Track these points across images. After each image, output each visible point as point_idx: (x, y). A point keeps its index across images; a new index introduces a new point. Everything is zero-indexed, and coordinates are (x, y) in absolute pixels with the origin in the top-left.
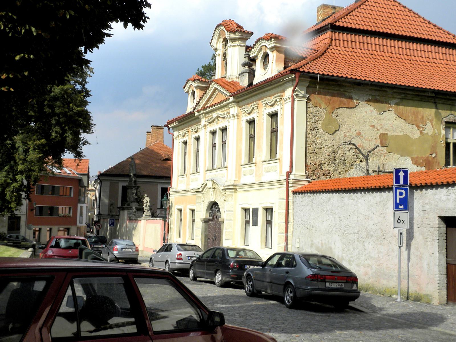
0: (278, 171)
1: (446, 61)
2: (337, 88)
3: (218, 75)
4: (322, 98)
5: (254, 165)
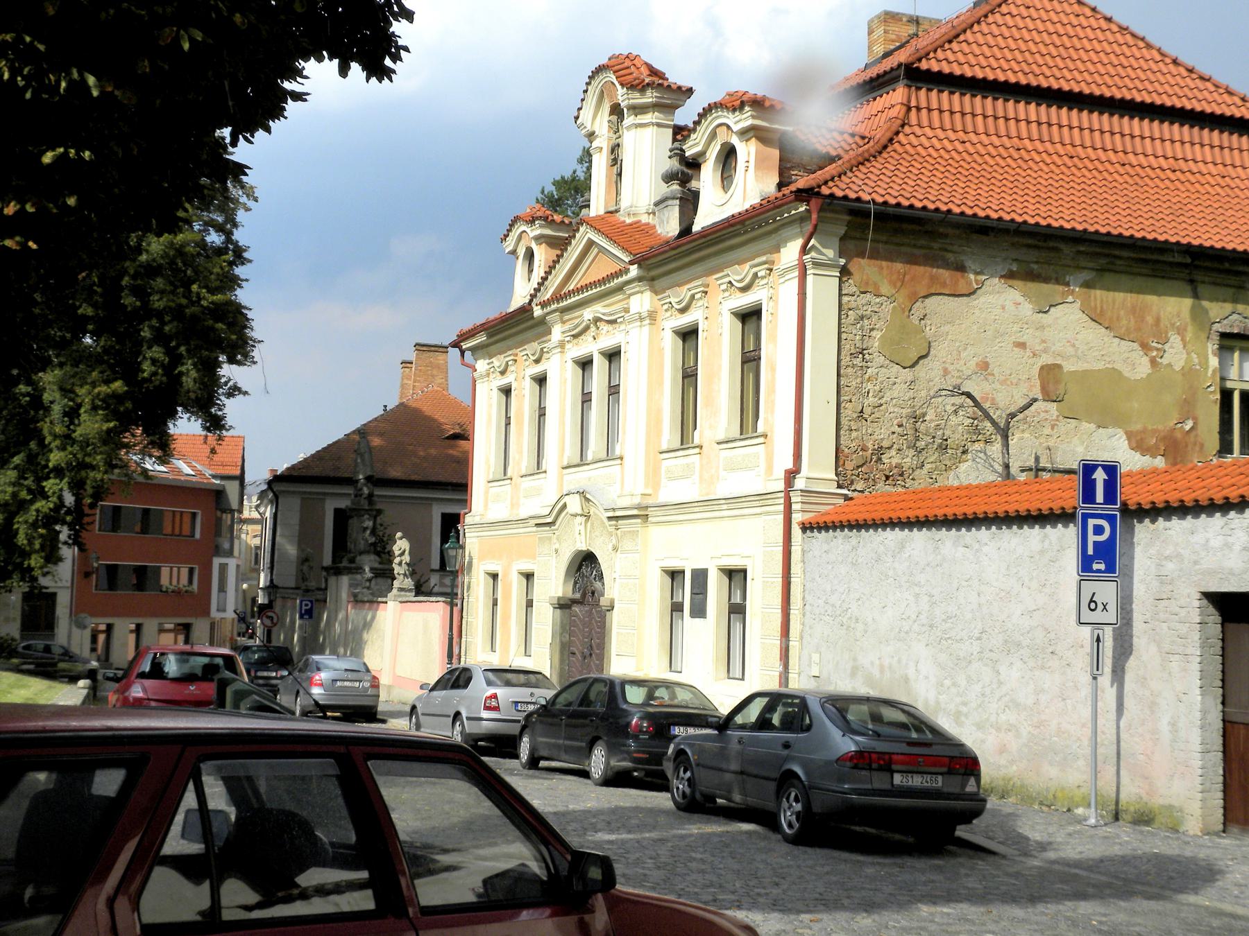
0: (761, 468)
1: (1220, 166)
3: (598, 204)
5: (697, 450)
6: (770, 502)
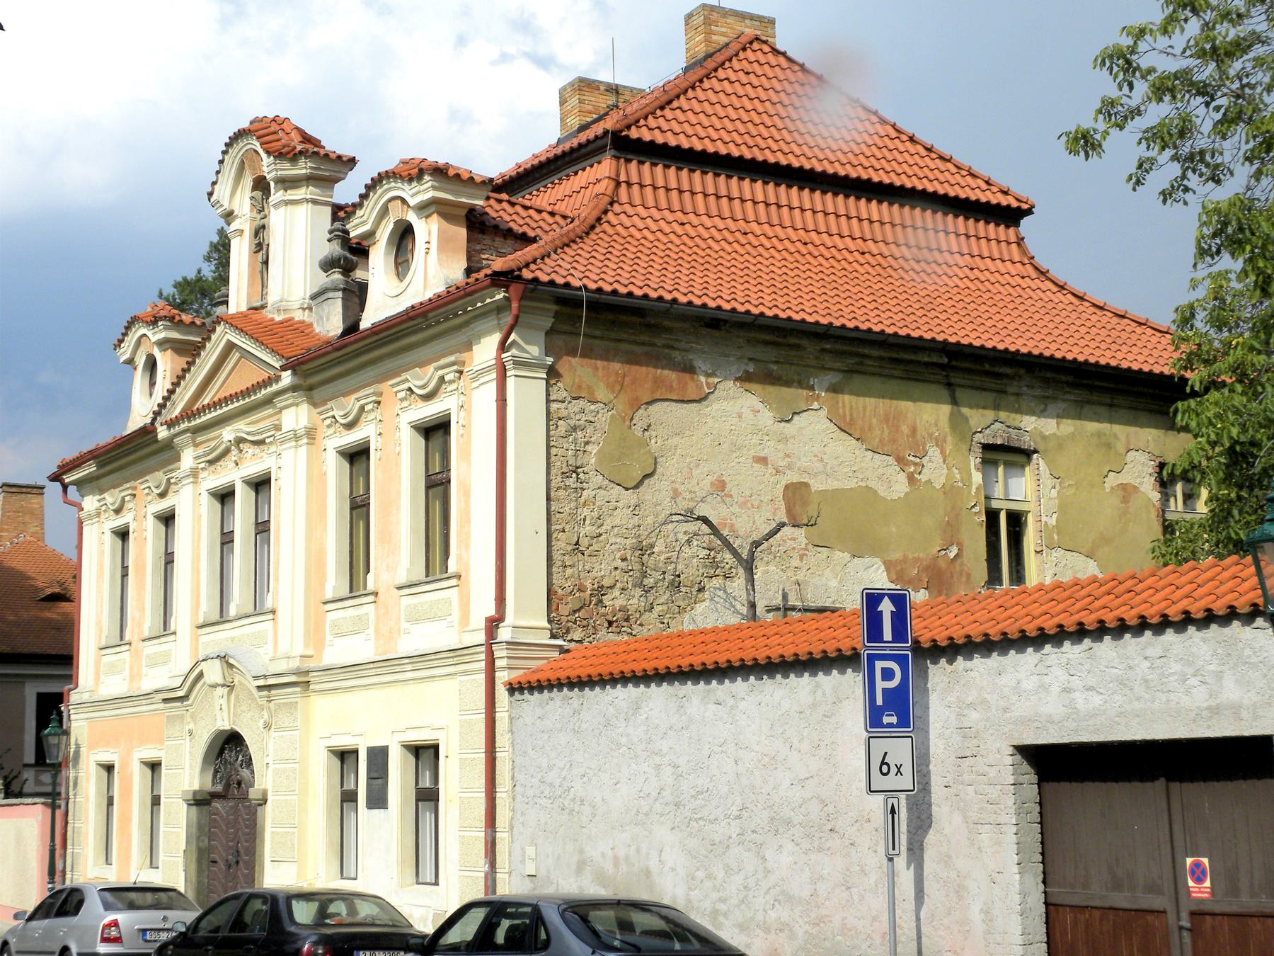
0: (455, 615)
1: (967, 257)
2: (644, 338)
3: (238, 298)
4: (596, 369)
5: (371, 598)
6: (467, 659)
